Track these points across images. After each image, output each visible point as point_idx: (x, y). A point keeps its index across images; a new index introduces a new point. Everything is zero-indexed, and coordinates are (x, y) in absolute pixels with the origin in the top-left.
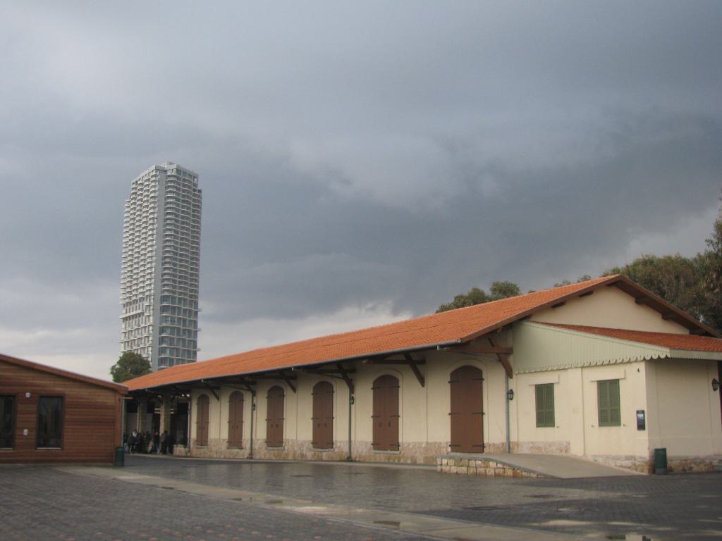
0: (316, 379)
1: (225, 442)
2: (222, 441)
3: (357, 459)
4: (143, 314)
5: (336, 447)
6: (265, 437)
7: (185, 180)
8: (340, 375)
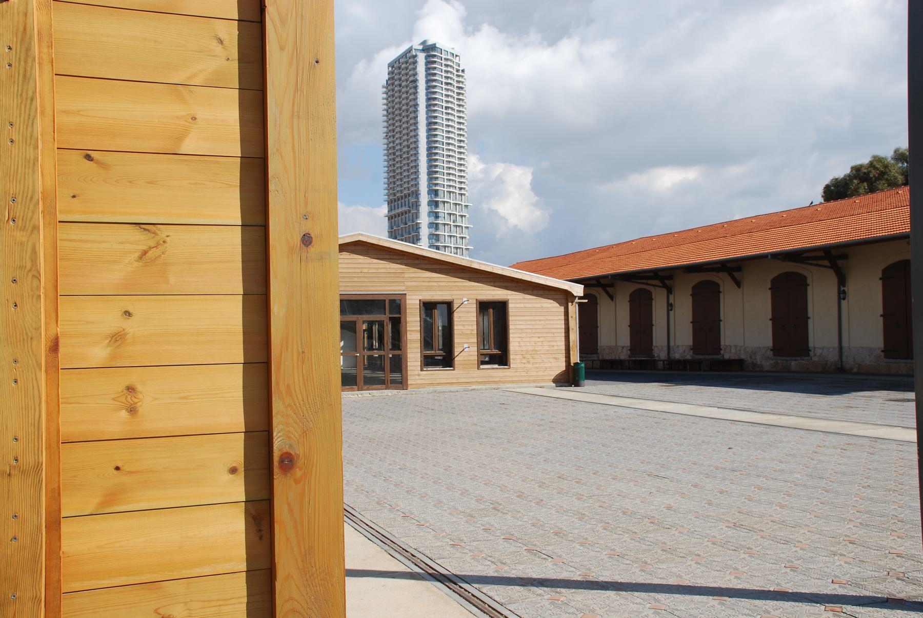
0: (634, 287)
1: (625, 349)
2: (620, 349)
3: (855, 370)
4: (409, 211)
5: (815, 355)
6: (690, 343)
7: (446, 59)
8: (826, 263)
